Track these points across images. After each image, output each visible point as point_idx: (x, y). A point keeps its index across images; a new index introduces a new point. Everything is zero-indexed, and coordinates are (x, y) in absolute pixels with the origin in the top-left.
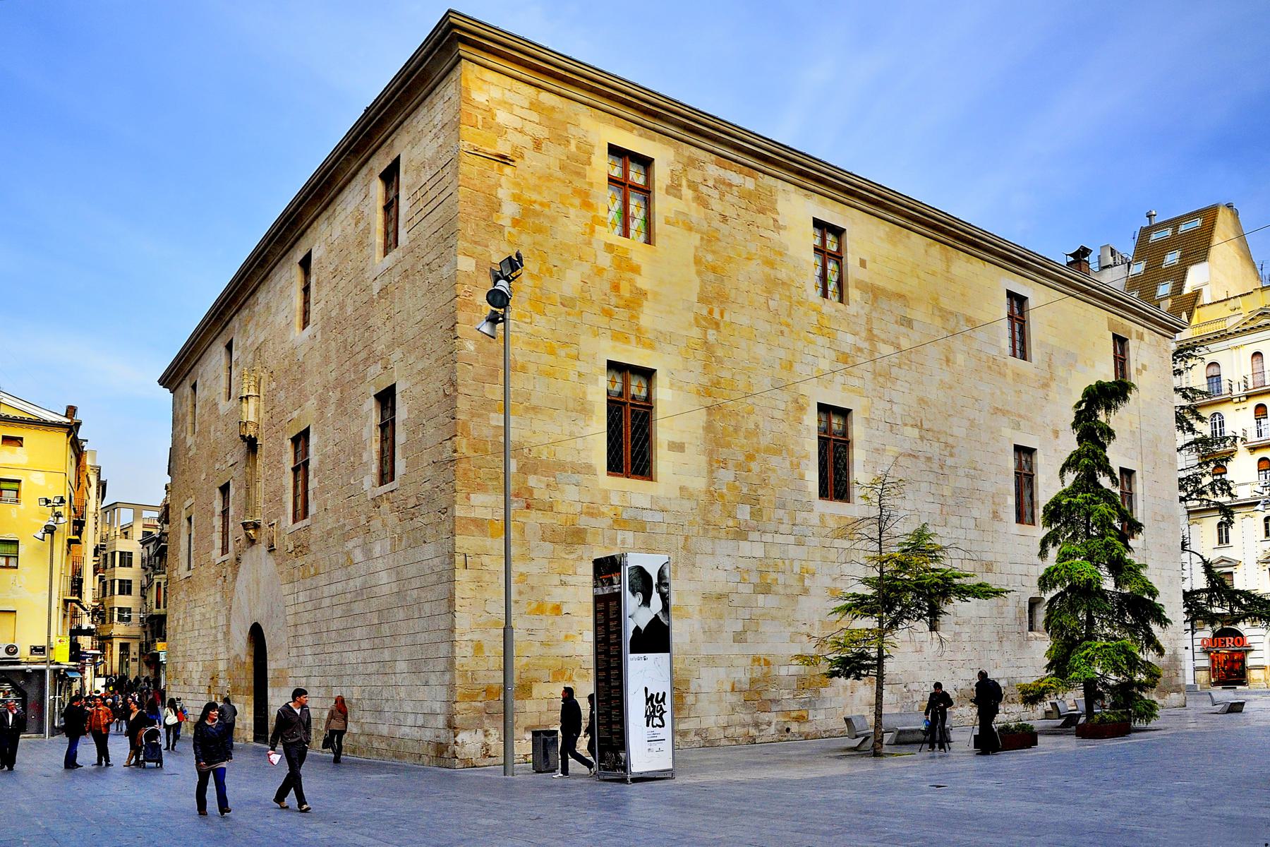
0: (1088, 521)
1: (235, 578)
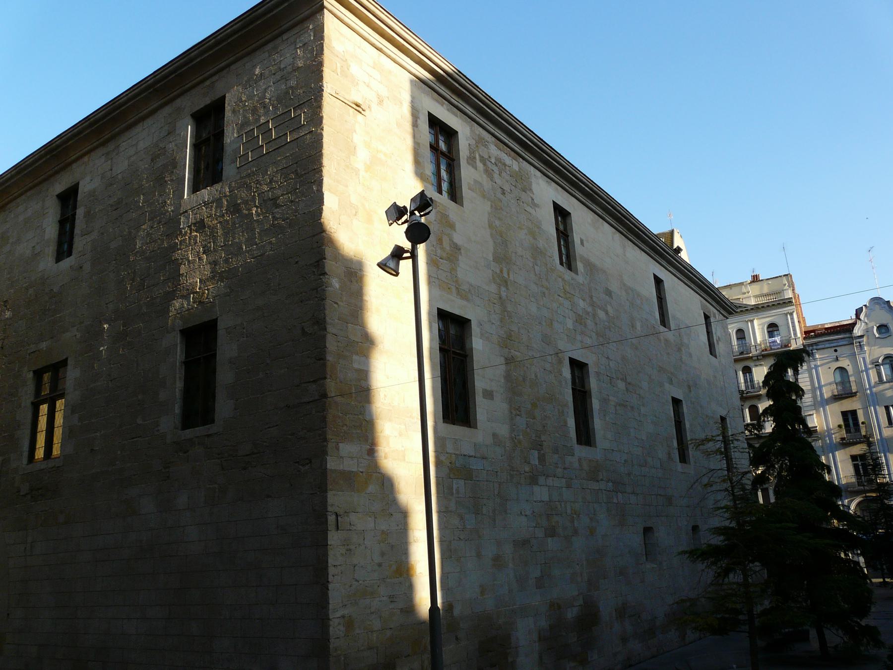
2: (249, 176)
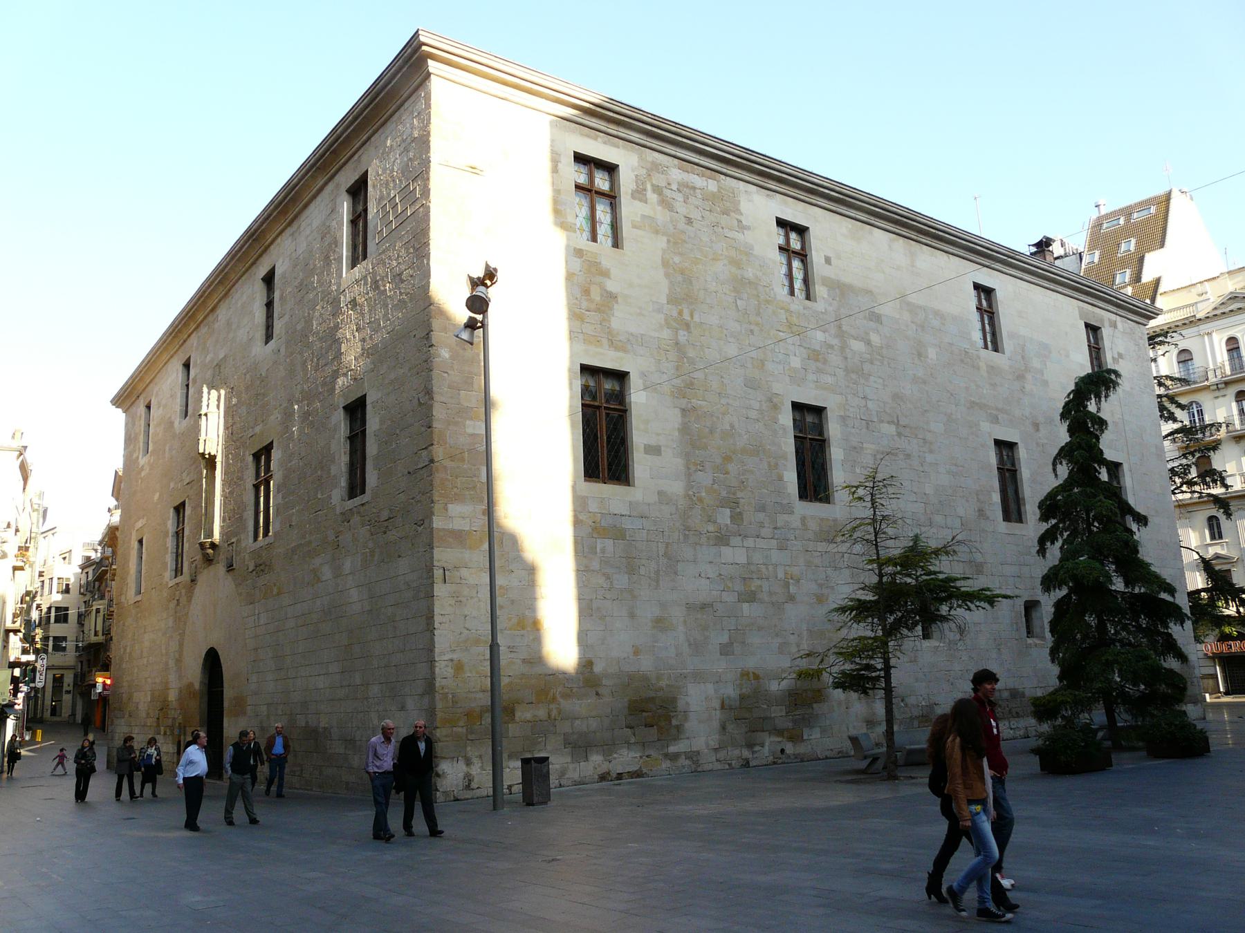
0: (1088, 517)
1: (189, 601)
2: (384, 252)
